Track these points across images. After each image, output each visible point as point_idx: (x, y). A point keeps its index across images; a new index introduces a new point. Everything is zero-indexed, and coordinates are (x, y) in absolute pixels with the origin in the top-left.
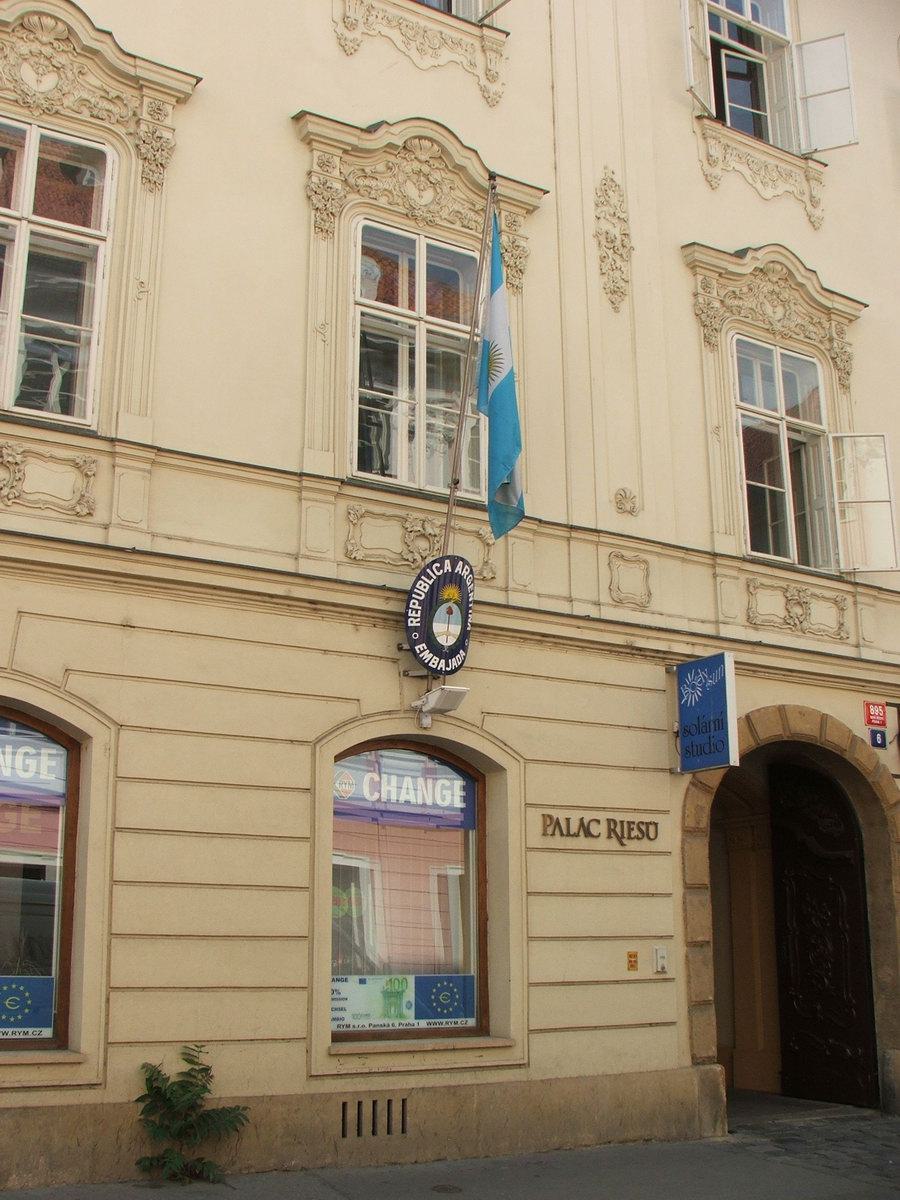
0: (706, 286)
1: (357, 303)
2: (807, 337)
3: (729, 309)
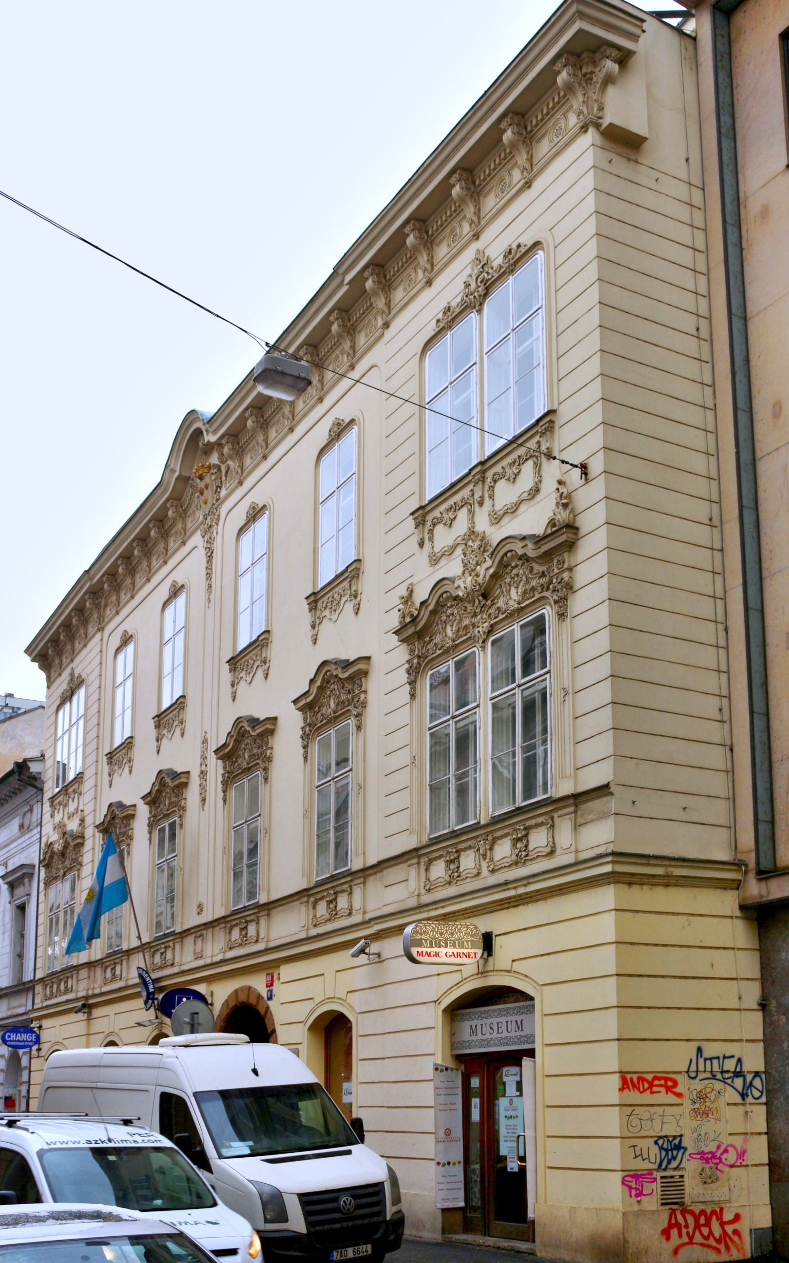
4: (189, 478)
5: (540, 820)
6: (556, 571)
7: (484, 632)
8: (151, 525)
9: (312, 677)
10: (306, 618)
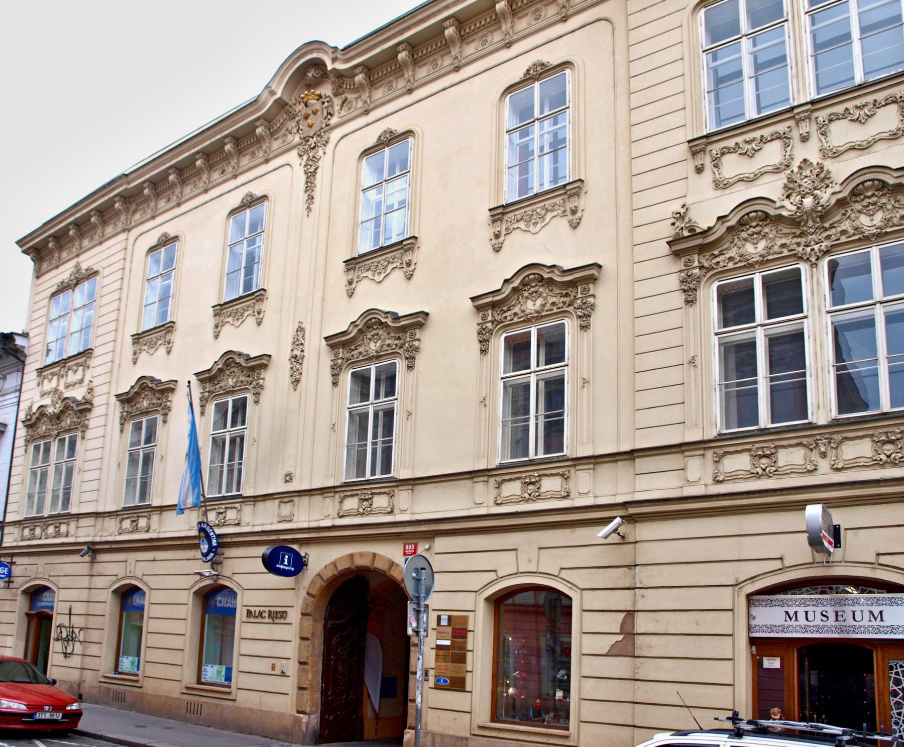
1: (828, 312)
2: (789, 251)
4: (287, 104)
5: (383, 490)
6: (408, 339)
7: (820, 251)
8: (71, 227)
9: (509, 277)
10: (485, 232)
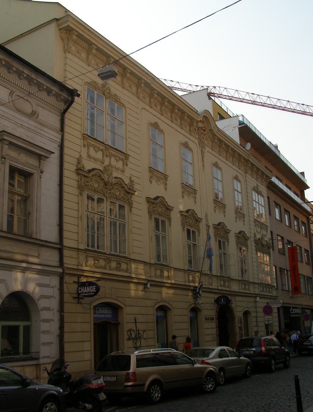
0: (81, 179)
3: (86, 186)
